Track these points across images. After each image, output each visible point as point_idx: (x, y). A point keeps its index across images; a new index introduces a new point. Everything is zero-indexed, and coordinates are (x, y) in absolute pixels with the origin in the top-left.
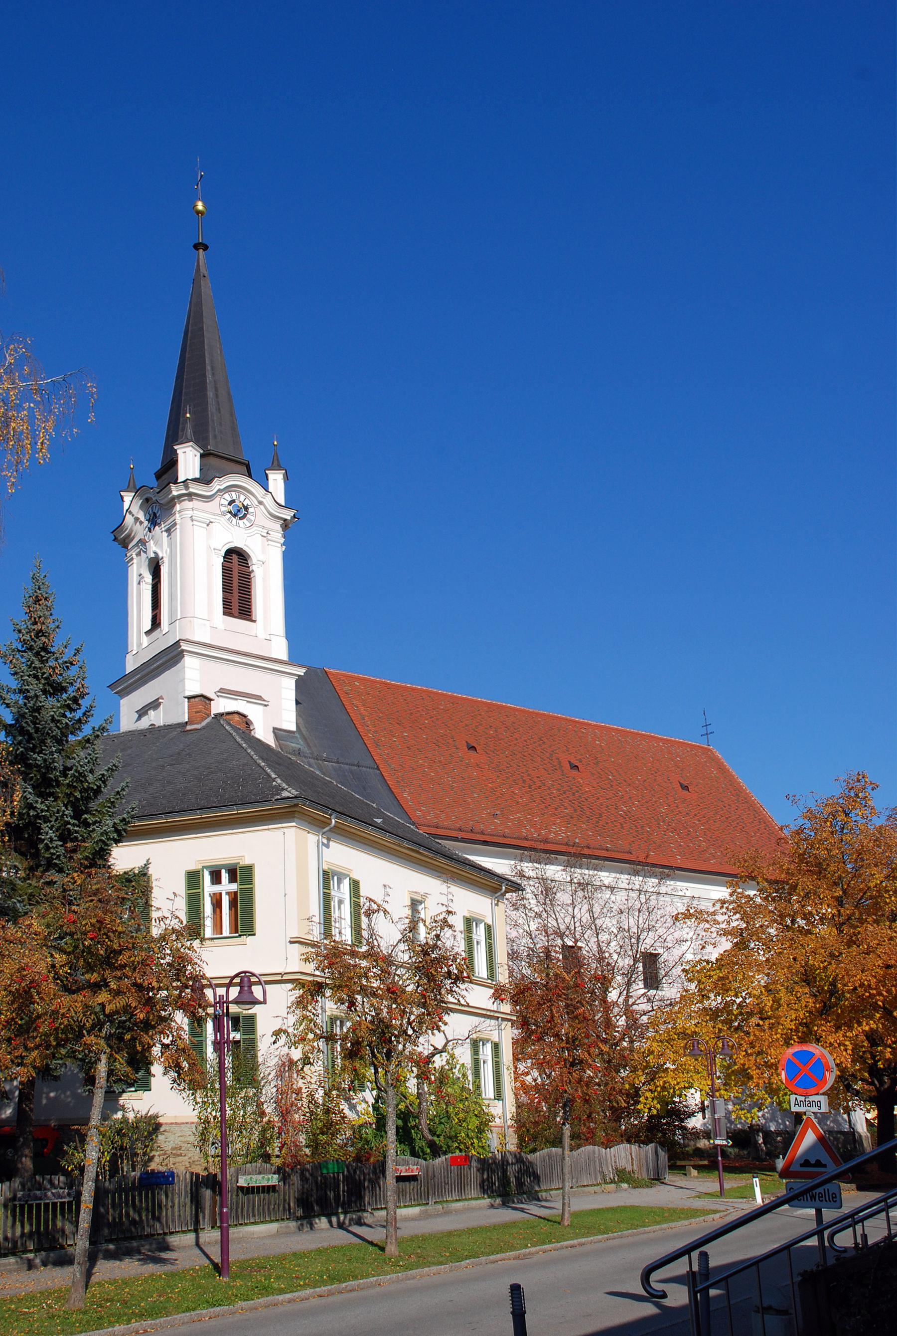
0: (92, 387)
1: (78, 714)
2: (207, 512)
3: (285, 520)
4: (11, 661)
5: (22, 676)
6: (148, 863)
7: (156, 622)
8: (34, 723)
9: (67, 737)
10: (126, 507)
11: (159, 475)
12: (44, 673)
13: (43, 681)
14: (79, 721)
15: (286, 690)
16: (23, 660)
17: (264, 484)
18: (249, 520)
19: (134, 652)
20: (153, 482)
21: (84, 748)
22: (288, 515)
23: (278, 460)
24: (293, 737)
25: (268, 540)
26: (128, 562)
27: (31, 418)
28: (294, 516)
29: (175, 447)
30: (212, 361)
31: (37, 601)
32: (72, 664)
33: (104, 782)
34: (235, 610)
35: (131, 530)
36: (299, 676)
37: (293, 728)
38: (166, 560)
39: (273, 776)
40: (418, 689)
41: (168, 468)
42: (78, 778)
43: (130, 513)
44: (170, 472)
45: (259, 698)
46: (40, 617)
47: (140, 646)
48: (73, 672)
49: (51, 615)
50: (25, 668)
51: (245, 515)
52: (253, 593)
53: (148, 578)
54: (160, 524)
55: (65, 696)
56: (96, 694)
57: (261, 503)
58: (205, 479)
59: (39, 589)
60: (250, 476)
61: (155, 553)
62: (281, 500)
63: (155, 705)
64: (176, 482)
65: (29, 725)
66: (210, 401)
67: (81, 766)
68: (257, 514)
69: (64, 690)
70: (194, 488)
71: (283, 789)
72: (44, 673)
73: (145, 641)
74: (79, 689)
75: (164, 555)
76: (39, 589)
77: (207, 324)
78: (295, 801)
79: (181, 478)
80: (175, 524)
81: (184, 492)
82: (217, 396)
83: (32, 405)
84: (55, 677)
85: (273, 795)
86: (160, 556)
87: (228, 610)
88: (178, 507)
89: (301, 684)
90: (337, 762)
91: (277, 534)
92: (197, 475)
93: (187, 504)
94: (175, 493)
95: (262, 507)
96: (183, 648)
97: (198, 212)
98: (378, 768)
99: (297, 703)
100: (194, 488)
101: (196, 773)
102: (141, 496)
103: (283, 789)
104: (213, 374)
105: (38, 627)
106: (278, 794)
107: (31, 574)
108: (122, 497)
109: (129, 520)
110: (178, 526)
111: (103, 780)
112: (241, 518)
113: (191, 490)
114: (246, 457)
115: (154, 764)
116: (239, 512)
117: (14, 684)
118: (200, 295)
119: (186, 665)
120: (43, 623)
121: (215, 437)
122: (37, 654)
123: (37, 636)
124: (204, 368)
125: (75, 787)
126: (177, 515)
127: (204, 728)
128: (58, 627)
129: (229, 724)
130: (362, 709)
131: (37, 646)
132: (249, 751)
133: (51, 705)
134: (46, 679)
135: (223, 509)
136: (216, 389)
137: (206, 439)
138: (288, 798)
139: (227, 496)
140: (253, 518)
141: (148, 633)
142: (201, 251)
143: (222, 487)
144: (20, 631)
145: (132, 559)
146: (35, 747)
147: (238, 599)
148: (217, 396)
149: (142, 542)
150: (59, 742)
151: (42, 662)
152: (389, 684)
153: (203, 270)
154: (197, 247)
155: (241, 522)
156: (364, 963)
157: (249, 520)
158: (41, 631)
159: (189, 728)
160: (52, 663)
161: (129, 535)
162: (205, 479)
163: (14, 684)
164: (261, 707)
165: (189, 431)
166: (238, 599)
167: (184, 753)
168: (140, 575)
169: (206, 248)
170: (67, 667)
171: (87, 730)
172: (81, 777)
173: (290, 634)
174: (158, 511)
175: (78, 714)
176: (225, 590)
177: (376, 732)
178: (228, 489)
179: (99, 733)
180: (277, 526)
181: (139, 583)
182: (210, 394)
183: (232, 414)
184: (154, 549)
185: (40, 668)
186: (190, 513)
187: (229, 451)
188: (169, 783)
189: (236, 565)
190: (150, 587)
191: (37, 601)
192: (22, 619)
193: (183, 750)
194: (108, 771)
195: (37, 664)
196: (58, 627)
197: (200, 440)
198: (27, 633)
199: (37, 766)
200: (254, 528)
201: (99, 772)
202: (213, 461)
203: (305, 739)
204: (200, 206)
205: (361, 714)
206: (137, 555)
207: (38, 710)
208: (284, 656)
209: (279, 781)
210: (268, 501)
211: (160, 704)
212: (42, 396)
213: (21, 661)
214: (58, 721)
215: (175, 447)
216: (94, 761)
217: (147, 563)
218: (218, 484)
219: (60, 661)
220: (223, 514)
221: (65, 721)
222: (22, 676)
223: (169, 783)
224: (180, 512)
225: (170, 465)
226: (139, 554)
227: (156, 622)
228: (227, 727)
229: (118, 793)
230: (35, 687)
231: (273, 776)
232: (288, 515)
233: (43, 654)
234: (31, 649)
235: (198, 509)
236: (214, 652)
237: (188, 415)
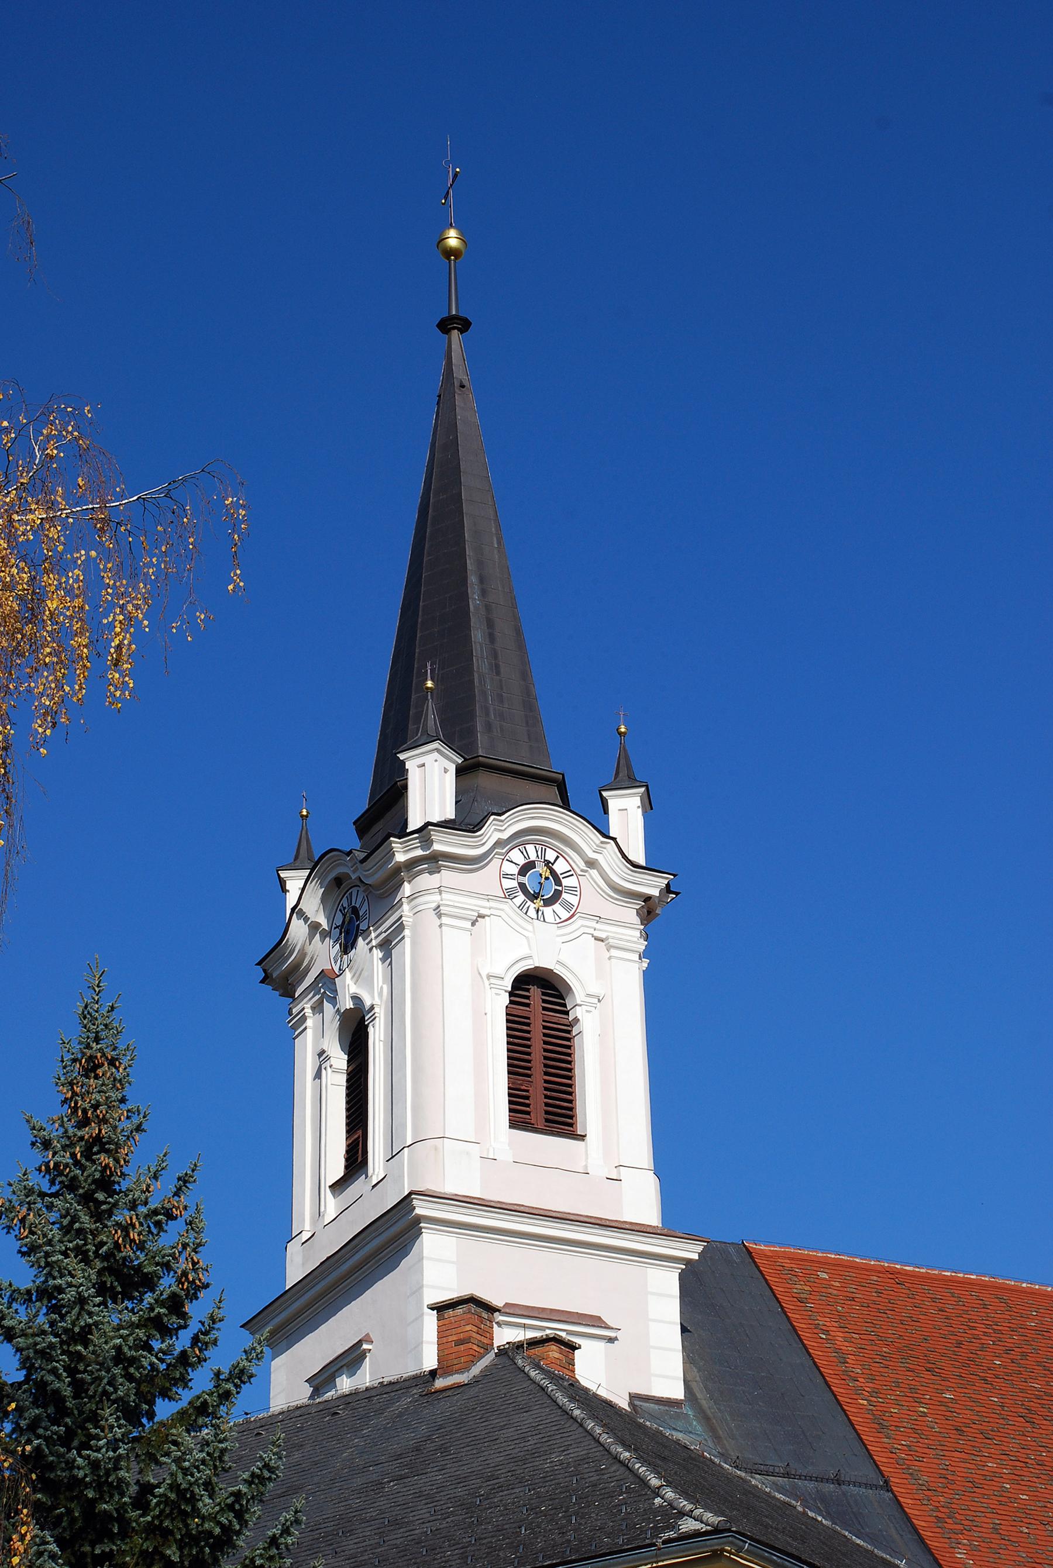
0: (236, 506)
1: (182, 1341)
2: (471, 894)
3: (647, 899)
4: (23, 1221)
5: (47, 1255)
6: (582, 1137)
7: (356, 1159)
8: (71, 1371)
9: (151, 1403)
10: (291, 900)
11: (363, 825)
12: (102, 1244)
13: (98, 1264)
14: (183, 1359)
15: (663, 1290)
16: (53, 1216)
18: (568, 906)
19: (305, 1236)
20: (350, 840)
21: (193, 1427)
22: (652, 885)
23: (629, 767)
24: (678, 1416)
25: (609, 947)
26: (294, 1028)
27: (93, 583)
28: (668, 889)
29: (402, 756)
30: (480, 564)
31: (91, 1069)
32: (170, 1217)
33: (240, 1515)
34: (538, 1115)
35: (303, 954)
36: (688, 1262)
37: (678, 1392)
38: (380, 1012)
39: (655, 1482)
40: (971, 1283)
41: (386, 804)
42: (175, 1505)
43: (301, 914)
44: (388, 815)
45: (596, 1321)
46: (95, 1107)
47: (320, 1220)
48: (173, 1234)
49: (123, 1100)
50: (55, 1232)
51: (557, 895)
52: (577, 1071)
53: (340, 1060)
54: (366, 933)
55: (149, 1298)
56: (228, 1300)
57: (591, 864)
58: (467, 820)
59: (97, 1040)
60: (566, 805)
61: (356, 998)
62: (639, 856)
63: (352, 1358)
64: (402, 833)
65: (58, 1377)
66: (476, 650)
67: (186, 1472)
68: (587, 892)
69: (149, 1282)
70: (444, 843)
71: (682, 1514)
72: (102, 1244)
73: (331, 1206)
74: (185, 1274)
75: (377, 1001)
76: (97, 1040)
77: (469, 481)
78: (715, 1543)
79: (415, 822)
80: (401, 928)
81: (419, 852)
82: (492, 638)
83: (93, 553)
84: (127, 1251)
85: (657, 1531)
86: (368, 1003)
87: (520, 1116)
88: (407, 889)
89: (694, 1283)
90: (787, 1475)
91: (631, 934)
92: (450, 814)
93: (426, 881)
94: (400, 857)
95: (594, 873)
96: (418, 1211)
97: (449, 253)
98: (887, 1486)
99: (684, 1330)
100: (444, 843)
101: (460, 1492)
102: (321, 878)
103: (682, 1514)
104: (484, 593)
105: (93, 1129)
106: (673, 1527)
107: (80, 1006)
108: (282, 883)
109: (298, 930)
110: (407, 932)
111: (237, 1507)
112: (548, 903)
113: (437, 847)
114: (556, 766)
115: (358, 1481)
116: (541, 889)
117: (25, 1276)
118: (453, 427)
119: (426, 1253)
120: (105, 1121)
121: (489, 727)
122: (87, 1199)
123: (88, 1154)
124: (465, 579)
125: (166, 1533)
126: (406, 907)
127: (476, 1381)
128: (139, 1128)
129: (537, 1366)
130: (839, 1336)
131: (86, 1174)
132: (590, 1425)
133: (114, 1320)
134: (106, 1257)
135: (509, 884)
136: (490, 624)
137: (471, 732)
138: (697, 1534)
139: (517, 856)
140: (573, 900)
141: (338, 1186)
142: (455, 333)
143: (505, 836)
144: (47, 1144)
145: (304, 1018)
146: (70, 1434)
147: (543, 1090)
148: (492, 638)
149: (327, 981)
150: (132, 1415)
151: (98, 1216)
152: (899, 1272)
153: (460, 374)
154: (445, 325)
155: (548, 911)
157: (568, 906)
158: (98, 1139)
159: (440, 1383)
160: (122, 1216)
161: (296, 966)
162: (467, 820)
163: (25, 1276)
164: (601, 1345)
165: (432, 719)
166: (543, 1090)
167: (430, 1446)
168: (323, 1052)
169: (464, 325)
170: (158, 1224)
171: (201, 1381)
172: (183, 1500)
173: (661, 1168)
174: (362, 905)
175: (182, 1341)
176: (514, 1069)
177: (876, 1393)
178: (519, 838)
179: (230, 1386)
180: (630, 914)
181: (318, 1075)
182: (478, 635)
183: (525, 676)
184: (353, 989)
185: (94, 1233)
186: (434, 899)
187: (520, 756)
188: (396, 1524)
189: (539, 1006)
190: (342, 1079)
191: (91, 1069)
192: (50, 1111)
193: (429, 1438)
194: (249, 1483)
195: (86, 1221)
196: (139, 1128)
197: (456, 735)
198: (64, 1148)
199: (76, 1483)
200: (578, 923)
201: (225, 1490)
202: (485, 781)
203: (705, 1418)
204: (453, 239)
205: (837, 1350)
206: (313, 1008)
207: (83, 1337)
208: (652, 1217)
209: (670, 1494)
210: (608, 858)
211: (363, 1356)
212: (115, 537)
213: (48, 1223)
214: (133, 1361)
215: (402, 756)
216: (217, 1460)
217: (336, 1024)
218: (494, 831)
219: (142, 1210)
220: (509, 895)
221: (147, 1360)
222: (47, 1255)
223: (396, 1524)
224: (411, 898)
225: (390, 795)
226: (318, 1008)
227: (356, 1159)
228: (533, 1374)
229: (274, 1541)
230: (81, 1278)
231: (655, 1482)
232: (652, 885)
233: (100, 1196)
234: (72, 1185)
235: (453, 890)
237: (429, 684)
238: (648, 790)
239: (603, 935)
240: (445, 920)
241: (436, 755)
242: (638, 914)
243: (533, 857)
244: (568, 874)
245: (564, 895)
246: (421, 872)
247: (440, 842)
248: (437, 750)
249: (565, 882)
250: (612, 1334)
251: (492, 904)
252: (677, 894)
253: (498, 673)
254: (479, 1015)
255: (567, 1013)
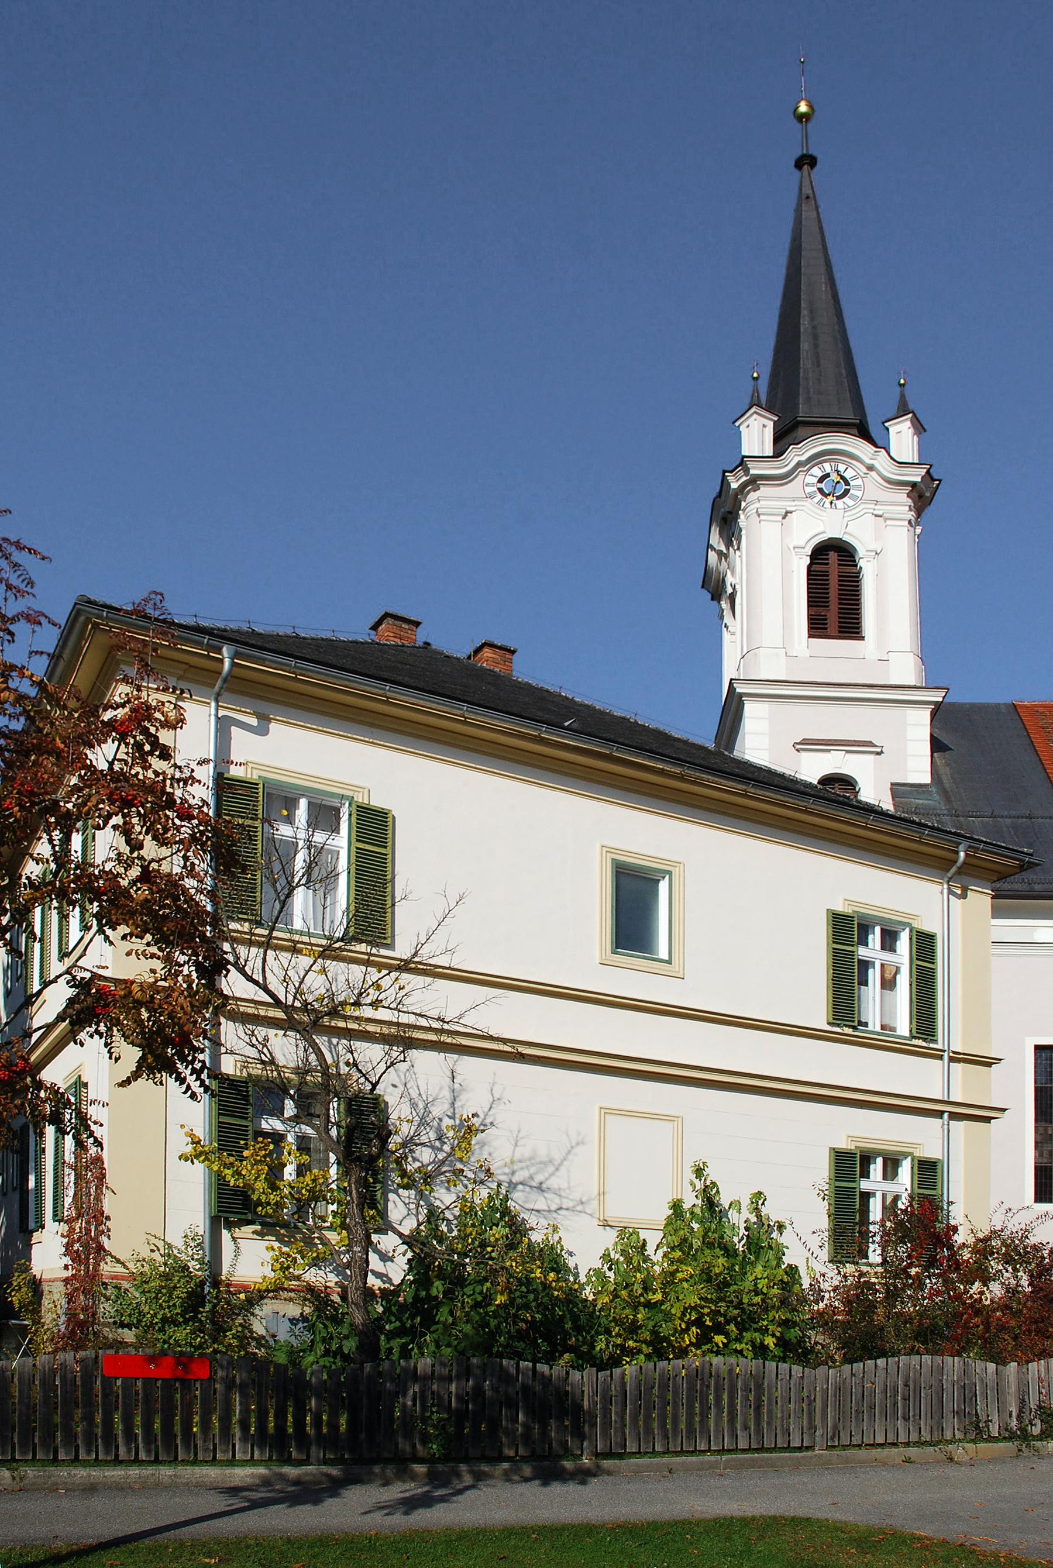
3: (914, 485)
15: (917, 726)
17: (880, 443)
22: (916, 475)
25: (886, 519)
36: (936, 703)
37: (926, 779)
45: (870, 744)
57: (871, 468)
66: (803, 355)
68: (868, 487)
81: (744, 479)
82: (816, 346)
87: (817, 627)
93: (752, 496)
94: (734, 485)
95: (873, 474)
96: (738, 690)
104: (812, 319)
113: (752, 472)
116: (835, 490)
121: (808, 399)
136: (815, 337)
139: (817, 472)
143: (804, 458)
148: (816, 346)
155: (839, 503)
156: (401, 1151)
157: (854, 498)
164: (872, 757)
178: (816, 459)
182: (805, 346)
218: (795, 455)
220: (811, 496)
235: (767, 498)
236: (788, 691)
238: (915, 415)
239: (880, 513)
240: (762, 517)
241: (755, 416)
242: (908, 496)
243: (828, 470)
244: (854, 478)
245: (851, 491)
246: (749, 492)
247: (754, 468)
248: (755, 412)
249: (852, 483)
250: (879, 750)
251: (796, 503)
252: (940, 481)
253: (819, 365)
254: (786, 574)
255: (856, 566)
